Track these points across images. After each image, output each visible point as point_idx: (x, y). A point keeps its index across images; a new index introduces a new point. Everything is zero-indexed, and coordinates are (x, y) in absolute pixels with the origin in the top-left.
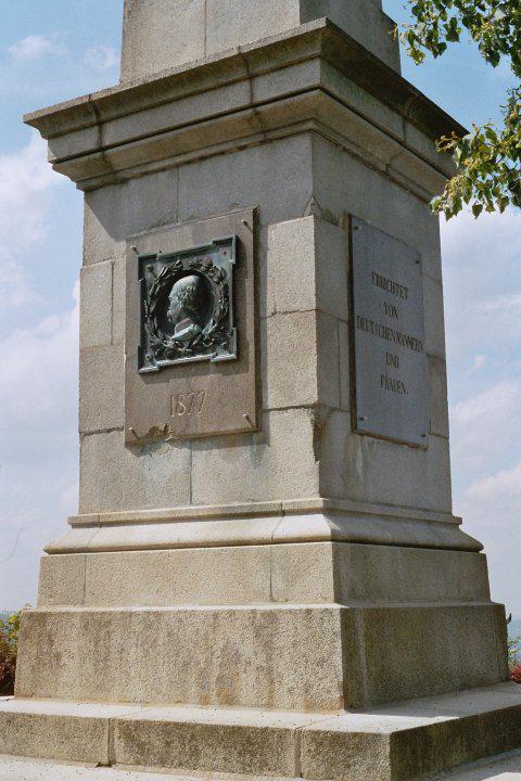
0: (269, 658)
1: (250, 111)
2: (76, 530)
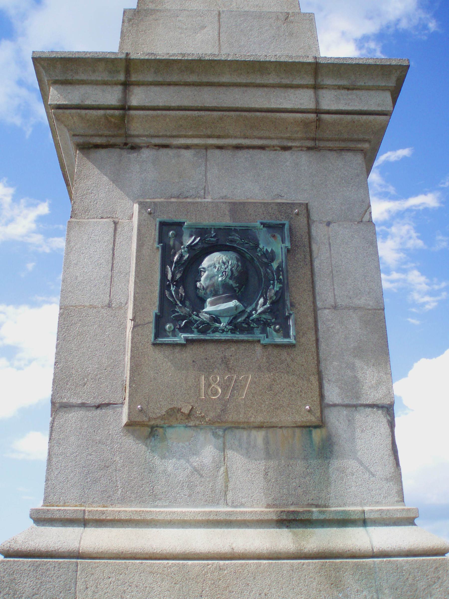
1: (313, 116)
2: (42, 528)
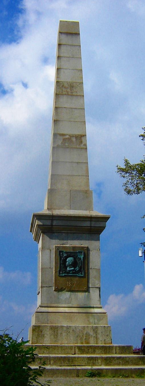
0: (96, 335)
1: (90, 228)
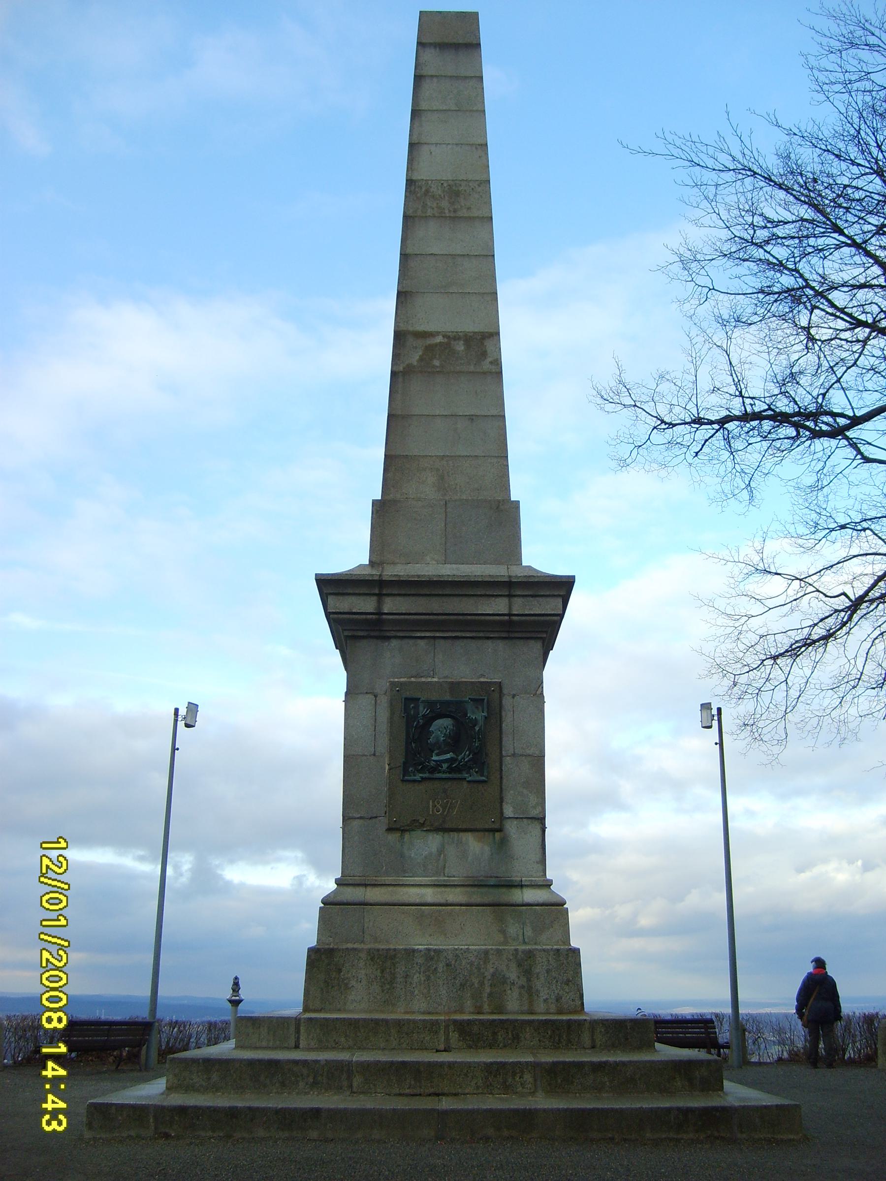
0: (529, 980)
1: (507, 618)
